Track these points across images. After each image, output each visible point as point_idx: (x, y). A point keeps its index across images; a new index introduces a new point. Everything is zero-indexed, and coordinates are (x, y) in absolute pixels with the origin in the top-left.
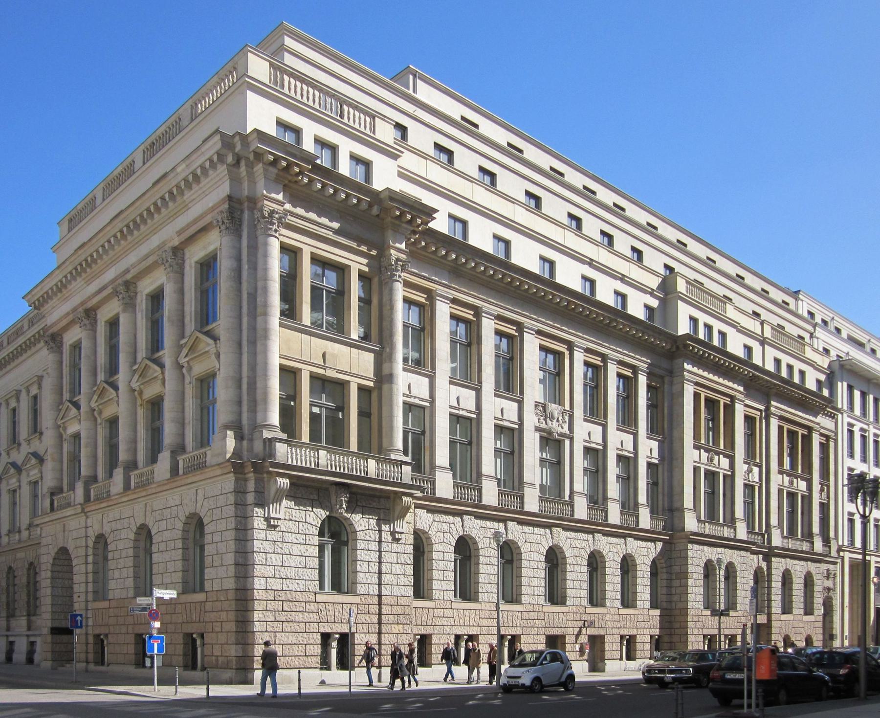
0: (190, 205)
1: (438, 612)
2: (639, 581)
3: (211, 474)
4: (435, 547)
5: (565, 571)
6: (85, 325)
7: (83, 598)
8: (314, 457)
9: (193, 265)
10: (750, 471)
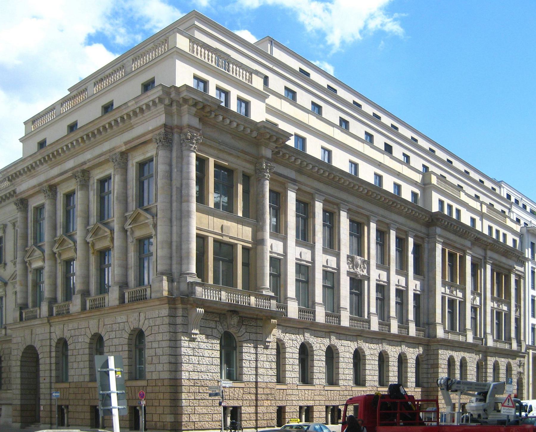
0: (135, 126)
1: (289, 392)
2: (409, 370)
3: (152, 304)
4: (288, 350)
5: (365, 364)
6: (49, 195)
7: (48, 380)
8: (218, 295)
9: (135, 164)
10: (474, 299)
